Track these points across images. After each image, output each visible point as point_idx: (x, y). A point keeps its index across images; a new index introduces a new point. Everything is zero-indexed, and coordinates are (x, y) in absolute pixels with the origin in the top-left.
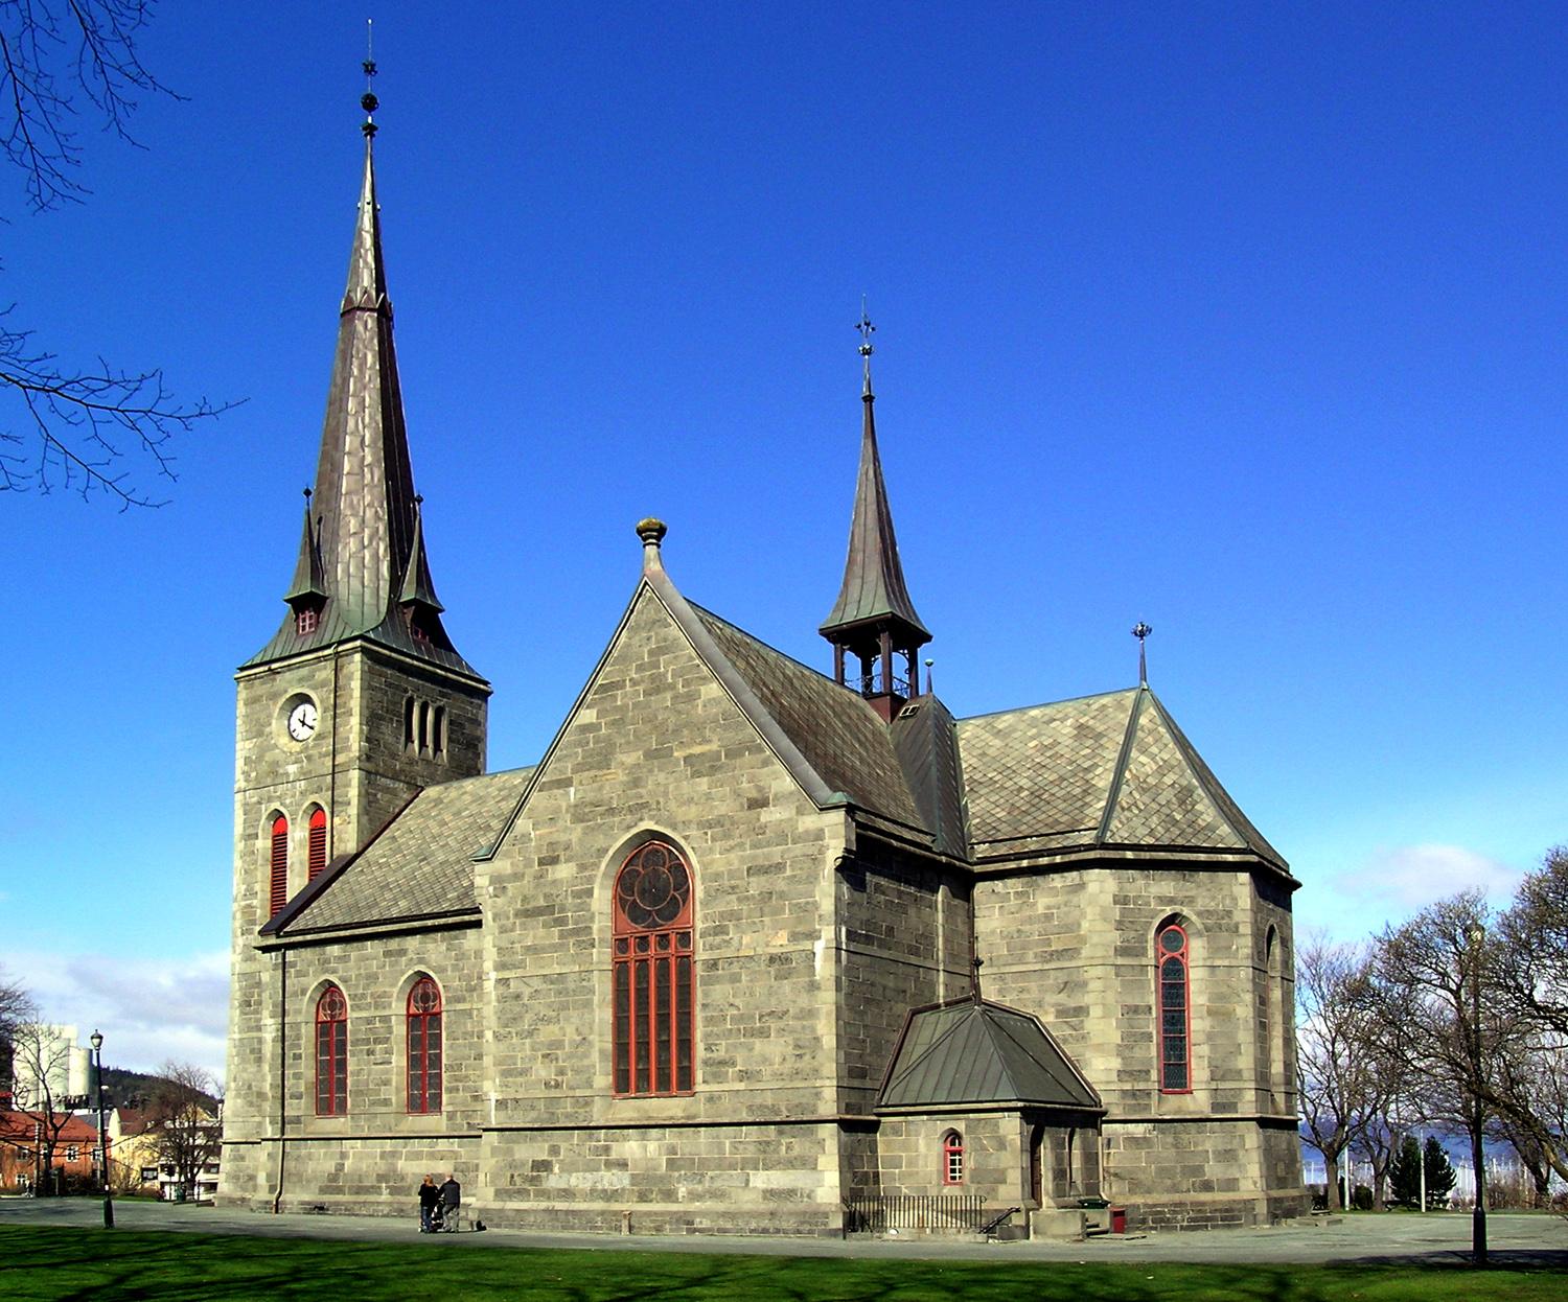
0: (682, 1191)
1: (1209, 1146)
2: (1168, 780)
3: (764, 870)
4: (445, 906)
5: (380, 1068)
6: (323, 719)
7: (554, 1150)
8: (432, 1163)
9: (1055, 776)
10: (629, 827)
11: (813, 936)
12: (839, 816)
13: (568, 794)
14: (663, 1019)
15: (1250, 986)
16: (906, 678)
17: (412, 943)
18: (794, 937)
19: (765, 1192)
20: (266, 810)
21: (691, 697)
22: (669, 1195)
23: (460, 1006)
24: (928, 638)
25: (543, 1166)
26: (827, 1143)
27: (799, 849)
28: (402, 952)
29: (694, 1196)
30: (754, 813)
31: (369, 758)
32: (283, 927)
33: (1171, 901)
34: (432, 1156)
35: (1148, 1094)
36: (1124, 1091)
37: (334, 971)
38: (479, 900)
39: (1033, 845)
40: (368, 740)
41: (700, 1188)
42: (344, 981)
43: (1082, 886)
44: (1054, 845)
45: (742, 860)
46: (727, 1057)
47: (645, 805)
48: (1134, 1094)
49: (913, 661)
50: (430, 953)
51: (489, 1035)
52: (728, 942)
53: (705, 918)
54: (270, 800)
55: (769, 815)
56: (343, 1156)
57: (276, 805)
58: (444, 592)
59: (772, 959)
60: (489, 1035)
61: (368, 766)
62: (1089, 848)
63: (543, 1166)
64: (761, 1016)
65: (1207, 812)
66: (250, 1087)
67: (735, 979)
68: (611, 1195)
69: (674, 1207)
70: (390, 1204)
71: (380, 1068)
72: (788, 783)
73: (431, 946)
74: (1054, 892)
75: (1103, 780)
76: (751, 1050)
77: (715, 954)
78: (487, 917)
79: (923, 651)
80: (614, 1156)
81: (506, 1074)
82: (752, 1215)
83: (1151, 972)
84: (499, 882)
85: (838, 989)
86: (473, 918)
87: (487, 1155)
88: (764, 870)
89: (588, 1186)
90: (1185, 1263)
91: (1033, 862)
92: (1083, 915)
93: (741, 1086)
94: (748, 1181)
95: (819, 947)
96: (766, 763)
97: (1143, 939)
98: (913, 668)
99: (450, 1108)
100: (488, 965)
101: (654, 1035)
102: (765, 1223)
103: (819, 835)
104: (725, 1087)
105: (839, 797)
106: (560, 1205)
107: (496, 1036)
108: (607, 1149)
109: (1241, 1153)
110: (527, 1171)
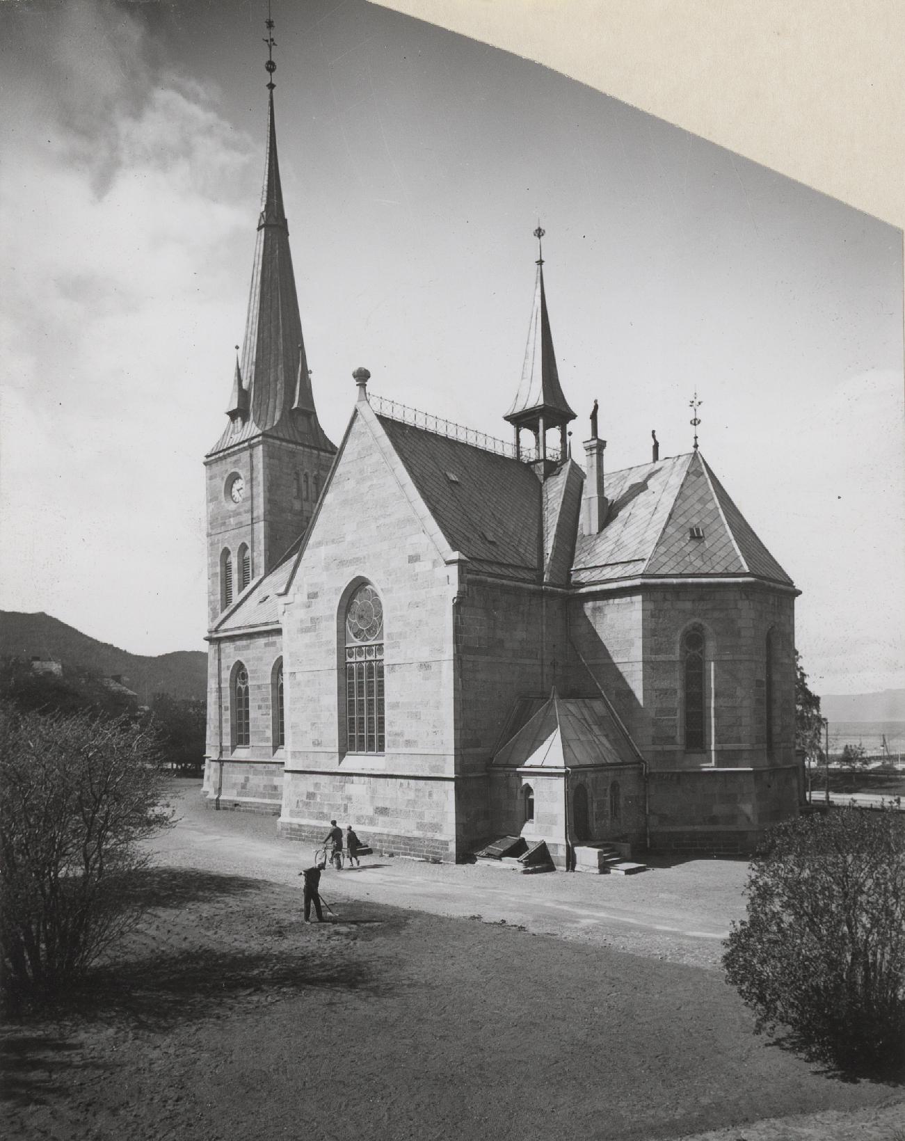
55: (420, 567)
63: (311, 796)
79: (571, 426)
110: (304, 798)
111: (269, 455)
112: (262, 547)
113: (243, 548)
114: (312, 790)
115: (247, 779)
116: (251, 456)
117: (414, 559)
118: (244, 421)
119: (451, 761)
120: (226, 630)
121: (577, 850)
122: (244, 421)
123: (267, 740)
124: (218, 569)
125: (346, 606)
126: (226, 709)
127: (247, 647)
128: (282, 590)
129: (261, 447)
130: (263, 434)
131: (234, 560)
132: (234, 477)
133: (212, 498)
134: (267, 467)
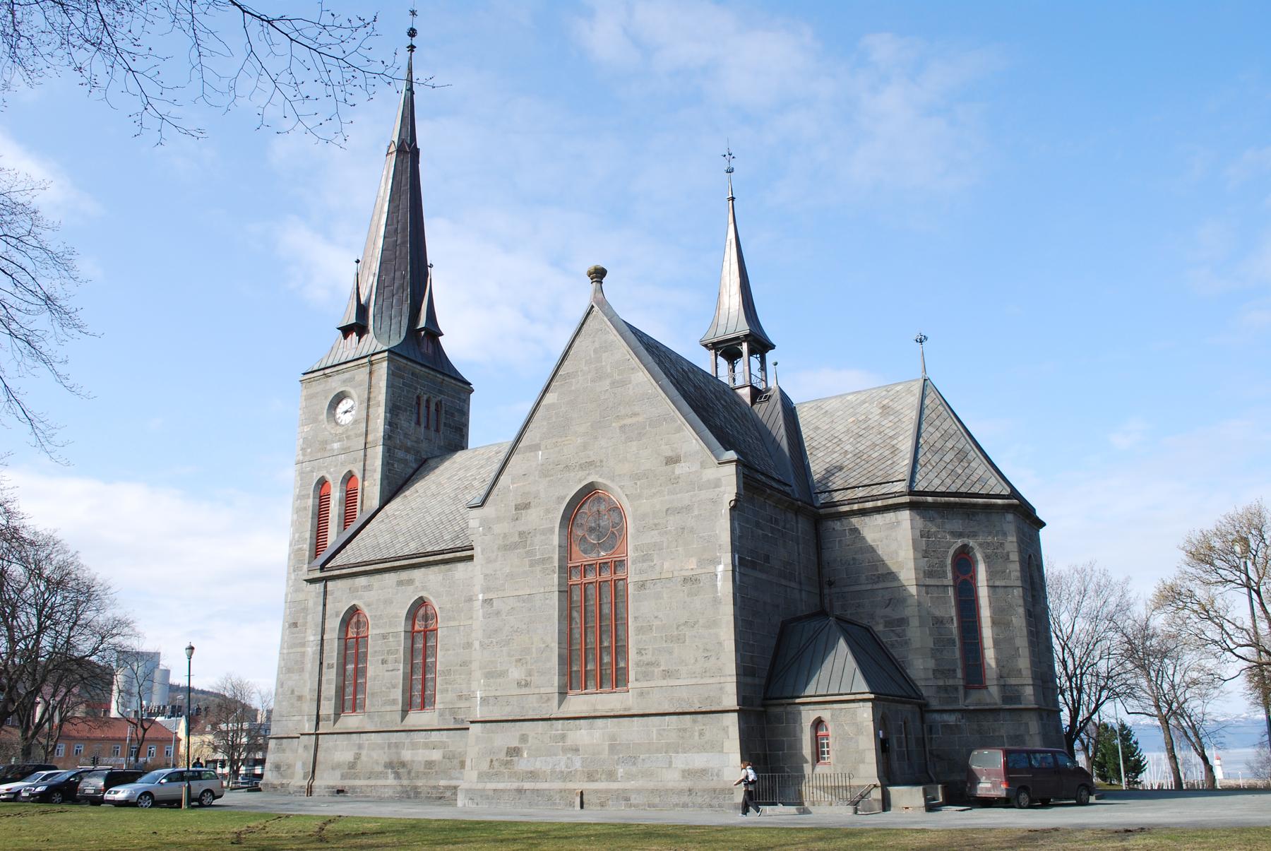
0: (621, 771)
1: (1003, 732)
2: (949, 445)
3: (679, 511)
4: (443, 546)
5: (384, 673)
7: (524, 738)
8: (427, 752)
9: (869, 443)
10: (580, 481)
11: (715, 561)
13: (537, 456)
15: (1021, 602)
16: (759, 375)
17: (417, 574)
18: (701, 563)
19: (683, 771)
21: (623, 383)
22: (611, 776)
23: (452, 623)
24: (773, 347)
25: (514, 752)
26: (731, 729)
27: (705, 495)
29: (629, 776)
30: (669, 468)
32: (324, 564)
33: (961, 535)
34: (426, 746)
35: (956, 688)
36: (939, 687)
37: (361, 598)
38: (471, 538)
39: (860, 493)
41: (634, 769)
44: (875, 492)
46: (653, 660)
47: (591, 463)
48: (945, 689)
49: (763, 362)
50: (428, 582)
51: (477, 645)
52: (653, 567)
53: (636, 549)
54: (319, 469)
55: (680, 469)
56: (360, 747)
58: (442, 323)
59: (685, 580)
60: (477, 645)
62: (902, 494)
63: (514, 752)
64: (678, 626)
65: (981, 469)
66: (293, 692)
68: (565, 776)
69: (614, 786)
70: (394, 787)
71: (384, 673)
73: (432, 577)
75: (906, 446)
76: (671, 653)
77: (644, 577)
78: (477, 552)
79: (770, 356)
80: (569, 742)
81: (489, 675)
82: (672, 791)
83: (951, 592)
84: (486, 524)
86: (469, 553)
87: (474, 743)
88: (679, 511)
89: (548, 768)
90: (1109, 831)
91: (861, 506)
93: (664, 683)
94: (671, 763)
95: (720, 568)
96: (679, 430)
97: (943, 564)
98: (763, 367)
99: (441, 706)
100: (477, 588)
101: (592, 643)
102: (685, 799)
103: (717, 484)
105: (732, 455)
106: (527, 785)
107: (481, 645)
108: (563, 737)
109: (1027, 738)
110: (502, 756)
111: (393, 374)
112: (378, 476)
113: (349, 477)
114: (515, 744)
115: (358, 756)
117: (672, 460)
118: (360, 336)
119: (731, 688)
120: (332, 569)
121: (893, 790)
122: (360, 336)
124: (310, 502)
126: (330, 666)
127: (368, 588)
128: (477, 501)
129: (385, 364)
130: (389, 350)
132: (340, 397)
133: (312, 419)
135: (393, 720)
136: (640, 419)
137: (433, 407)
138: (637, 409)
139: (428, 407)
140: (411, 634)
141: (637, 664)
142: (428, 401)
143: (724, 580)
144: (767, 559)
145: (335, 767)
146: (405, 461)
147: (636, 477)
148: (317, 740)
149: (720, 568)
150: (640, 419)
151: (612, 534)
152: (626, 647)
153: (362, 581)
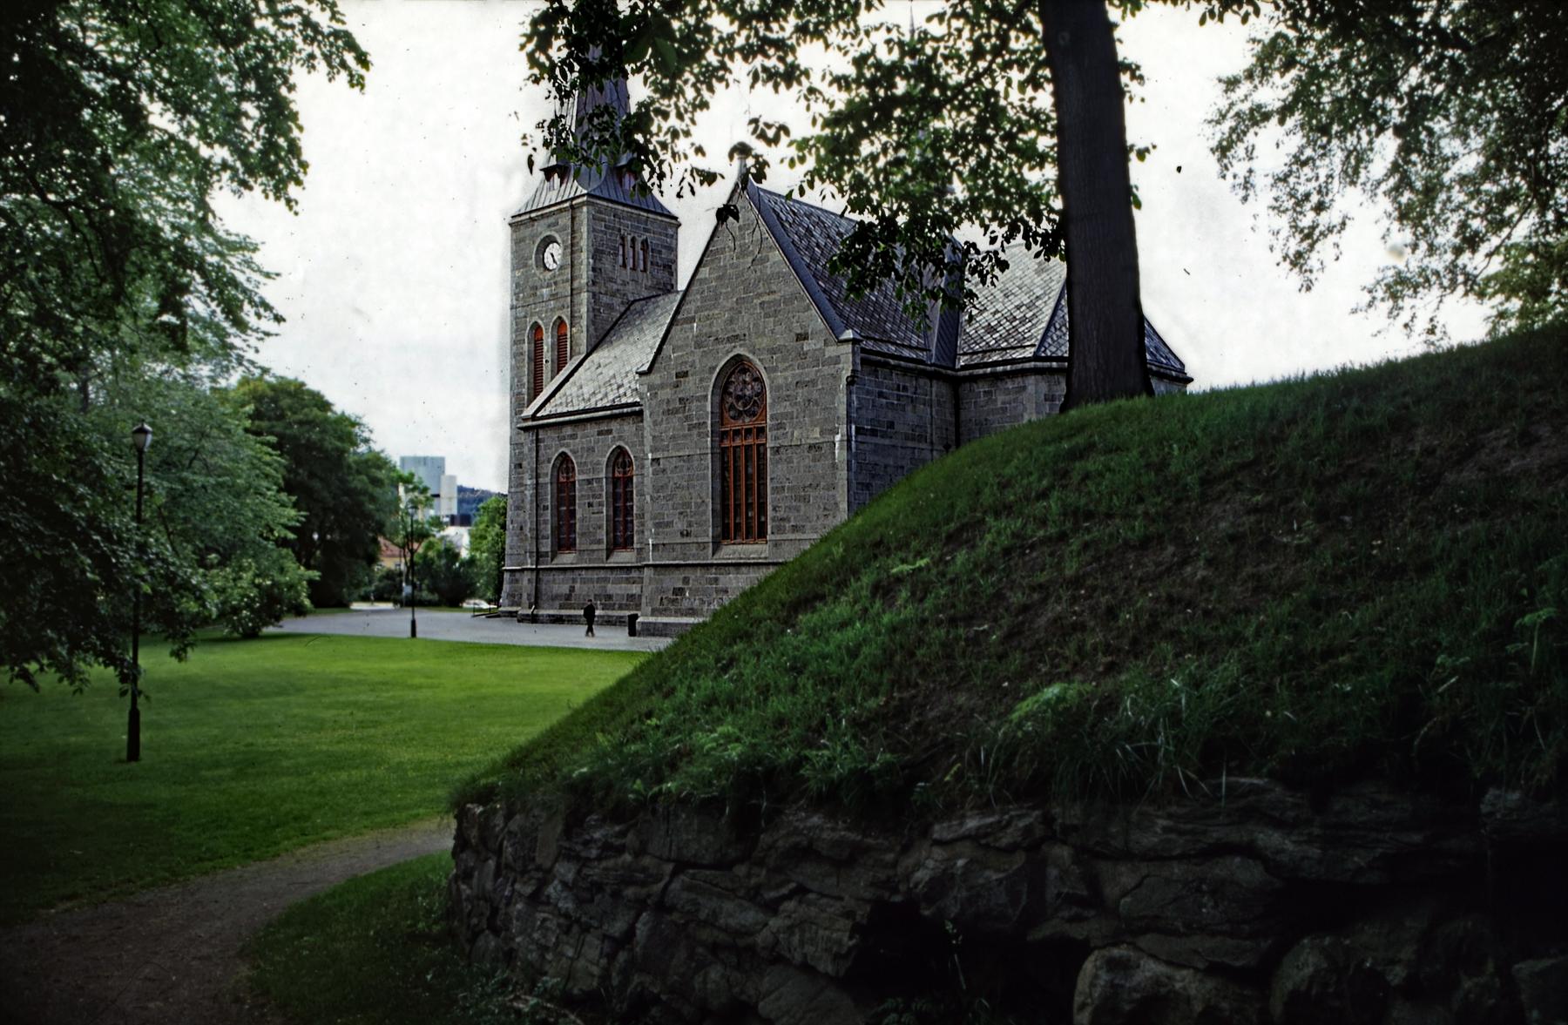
5: (592, 516)
6: (564, 255)
7: (686, 580)
12: (848, 348)
14: (749, 488)
20: (530, 322)
27: (827, 370)
28: (609, 432)
31: (594, 283)
34: (628, 581)
37: (568, 446)
40: (594, 270)
42: (574, 452)
43: (1024, 388)
45: (794, 376)
53: (772, 418)
55: (808, 346)
56: (574, 580)
57: (535, 319)
59: (811, 447)
61: (596, 289)
67: (790, 461)
71: (592, 516)
72: (819, 323)
74: (1007, 392)
81: (657, 525)
85: (849, 469)
92: (1025, 409)
95: (838, 438)
100: (647, 448)
104: (784, 537)
108: (716, 580)
113: (560, 323)
114: (680, 585)
115: (572, 589)
116: (573, 219)
117: (802, 337)
123: (599, 542)
125: (723, 387)
127: (573, 437)
128: (645, 368)
130: (588, 195)
131: (548, 341)
132: (548, 241)
134: (592, 230)
135: (599, 559)
136: (777, 296)
137: (638, 246)
138: (774, 288)
139: (633, 247)
140: (615, 482)
141: (773, 519)
142: (633, 240)
143: (841, 448)
144: (891, 425)
145: (554, 598)
146: (610, 307)
147: (772, 351)
148: (538, 581)
149: (838, 438)
150: (777, 296)
151: (755, 404)
152: (765, 504)
153: (568, 431)
